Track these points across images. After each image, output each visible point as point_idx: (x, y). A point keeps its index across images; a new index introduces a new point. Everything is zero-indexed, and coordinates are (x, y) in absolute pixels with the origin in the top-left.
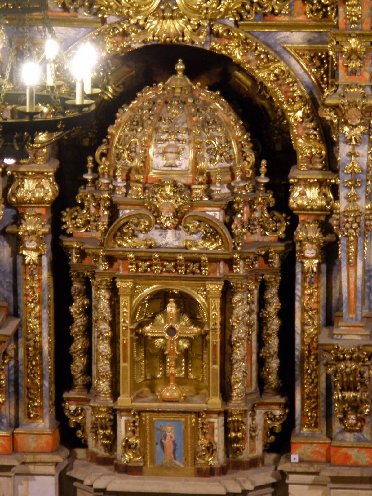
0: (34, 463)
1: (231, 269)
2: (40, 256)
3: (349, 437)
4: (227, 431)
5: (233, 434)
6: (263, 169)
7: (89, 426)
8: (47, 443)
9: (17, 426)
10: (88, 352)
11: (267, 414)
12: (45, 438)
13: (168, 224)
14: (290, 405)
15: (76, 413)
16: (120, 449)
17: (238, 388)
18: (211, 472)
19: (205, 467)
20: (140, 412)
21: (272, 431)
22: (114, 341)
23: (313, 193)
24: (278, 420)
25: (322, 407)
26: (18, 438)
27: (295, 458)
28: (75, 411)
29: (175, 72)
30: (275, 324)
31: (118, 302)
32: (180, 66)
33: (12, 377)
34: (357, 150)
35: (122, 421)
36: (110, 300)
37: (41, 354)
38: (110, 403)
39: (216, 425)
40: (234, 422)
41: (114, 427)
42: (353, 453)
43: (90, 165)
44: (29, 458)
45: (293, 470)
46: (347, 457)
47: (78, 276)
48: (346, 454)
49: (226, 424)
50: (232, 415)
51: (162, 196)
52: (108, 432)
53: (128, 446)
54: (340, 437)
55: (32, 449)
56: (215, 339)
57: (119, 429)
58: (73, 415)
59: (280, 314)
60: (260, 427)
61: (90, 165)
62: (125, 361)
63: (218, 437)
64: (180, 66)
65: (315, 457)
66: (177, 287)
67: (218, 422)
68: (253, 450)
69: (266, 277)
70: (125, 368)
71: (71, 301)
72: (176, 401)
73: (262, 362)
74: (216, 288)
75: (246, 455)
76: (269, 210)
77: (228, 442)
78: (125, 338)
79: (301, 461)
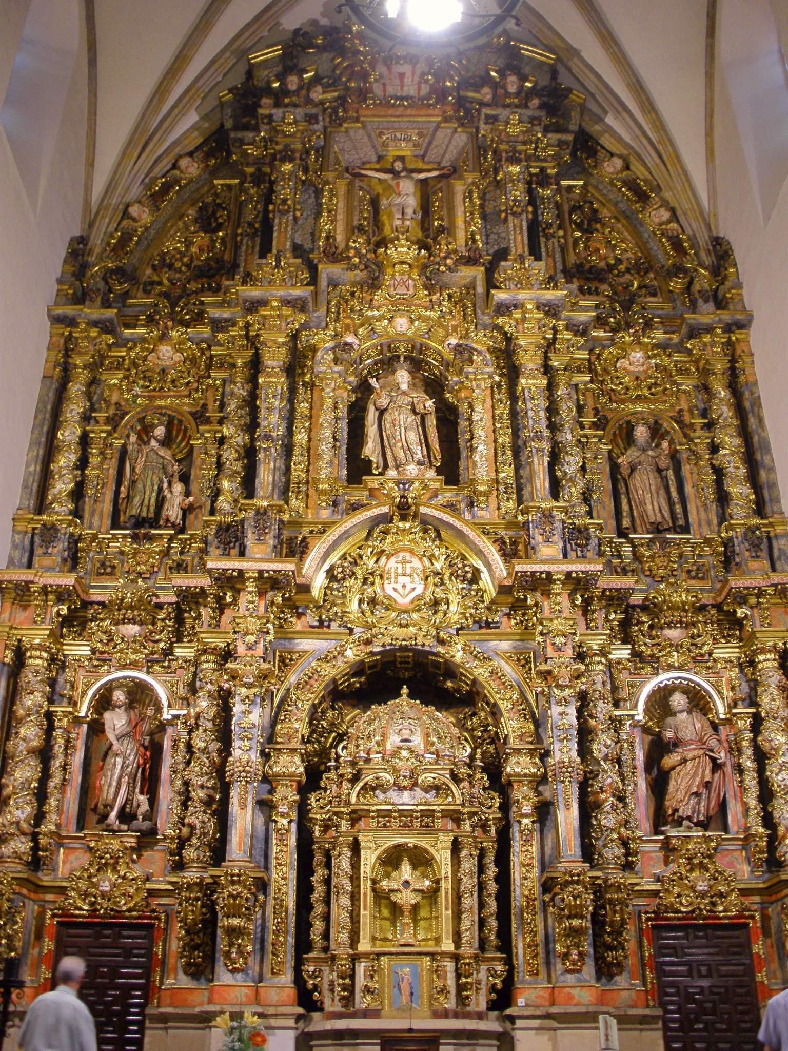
0: (276, 1015)
1: (459, 827)
2: (290, 822)
3: (570, 977)
4: (458, 976)
5: (464, 980)
6: (478, 756)
7: (326, 986)
8: (288, 995)
9: (260, 981)
10: (327, 918)
11: (488, 970)
12: (287, 991)
13: (406, 783)
14: (509, 962)
15: (314, 976)
16: (358, 995)
17: (466, 936)
18: (445, 1014)
19: (440, 1008)
20: (379, 955)
21: (493, 988)
22: (354, 897)
23: (524, 760)
24: (500, 976)
25: (542, 954)
26: (261, 991)
27: (521, 1001)
28: (314, 972)
29: (401, 695)
30: (493, 887)
31: (359, 856)
32: (405, 690)
33: (259, 935)
34: (567, 710)
35: (361, 968)
36: (351, 858)
37: (286, 912)
38: (351, 952)
39: (449, 969)
40: (465, 964)
41: (352, 977)
42: (576, 992)
43: (333, 755)
44: (271, 1011)
45: (520, 1013)
46: (570, 997)
47: (319, 848)
48: (569, 994)
49: (457, 969)
50: (464, 958)
51: (400, 759)
52: (347, 981)
53: (367, 990)
54: (562, 978)
55: (274, 1002)
56: (446, 886)
57: (357, 977)
58: (310, 977)
59: (497, 879)
60: (484, 983)
61: (333, 755)
62: (365, 909)
63: (451, 982)
64: (405, 690)
65: (539, 1001)
66: (410, 840)
67: (450, 966)
68: (477, 1005)
69: (485, 844)
70: (365, 915)
71: (312, 873)
72: (412, 946)
73: (482, 923)
74: (446, 840)
75: (472, 1008)
76: (485, 789)
77: (460, 988)
78: (366, 887)
79: (527, 1005)
